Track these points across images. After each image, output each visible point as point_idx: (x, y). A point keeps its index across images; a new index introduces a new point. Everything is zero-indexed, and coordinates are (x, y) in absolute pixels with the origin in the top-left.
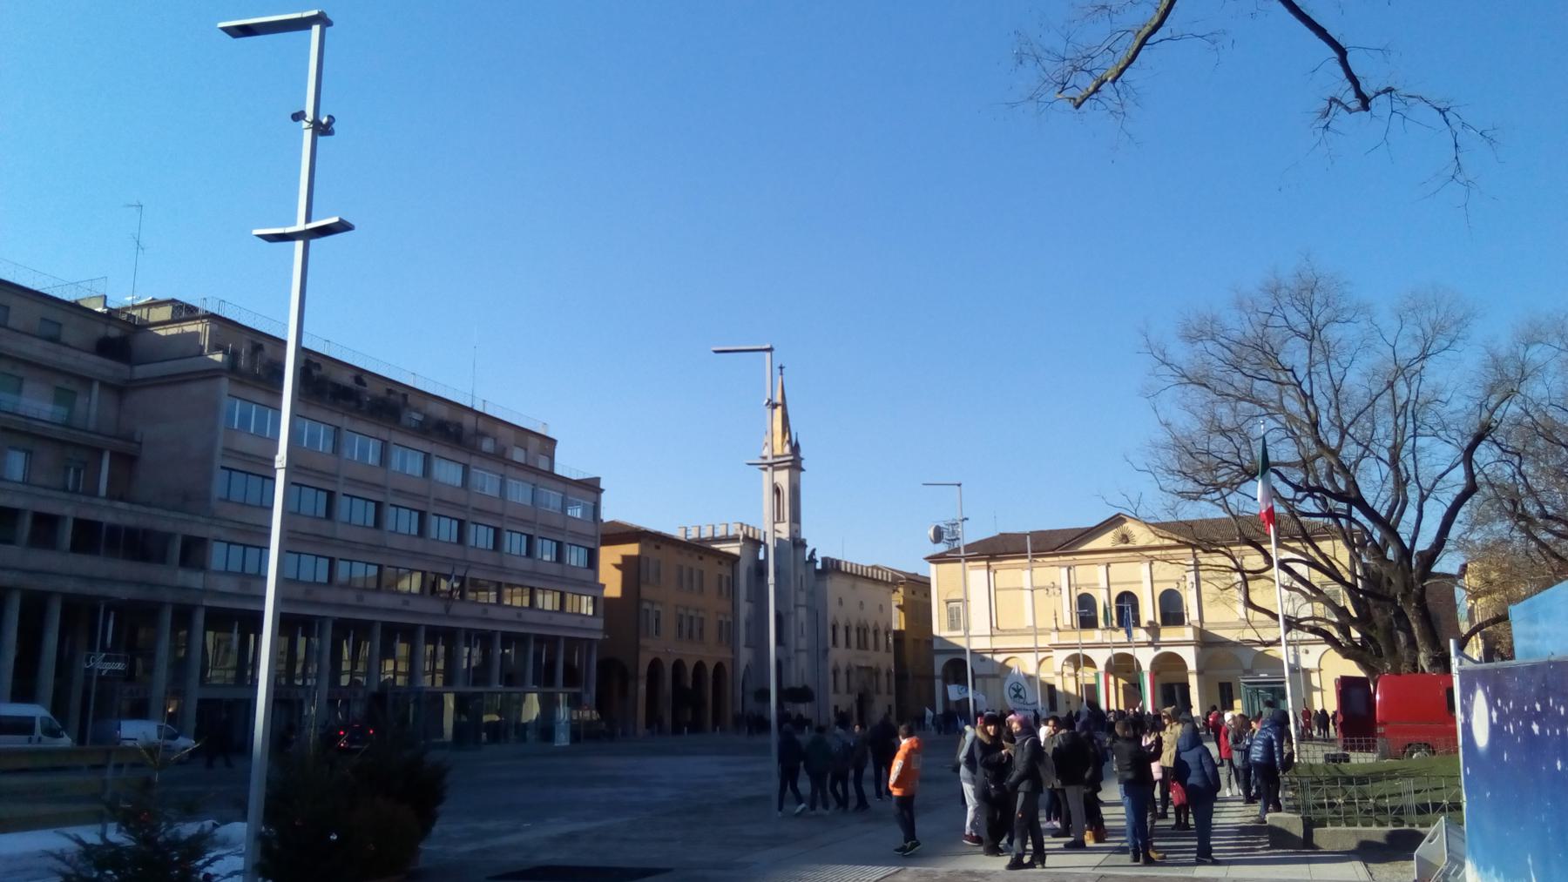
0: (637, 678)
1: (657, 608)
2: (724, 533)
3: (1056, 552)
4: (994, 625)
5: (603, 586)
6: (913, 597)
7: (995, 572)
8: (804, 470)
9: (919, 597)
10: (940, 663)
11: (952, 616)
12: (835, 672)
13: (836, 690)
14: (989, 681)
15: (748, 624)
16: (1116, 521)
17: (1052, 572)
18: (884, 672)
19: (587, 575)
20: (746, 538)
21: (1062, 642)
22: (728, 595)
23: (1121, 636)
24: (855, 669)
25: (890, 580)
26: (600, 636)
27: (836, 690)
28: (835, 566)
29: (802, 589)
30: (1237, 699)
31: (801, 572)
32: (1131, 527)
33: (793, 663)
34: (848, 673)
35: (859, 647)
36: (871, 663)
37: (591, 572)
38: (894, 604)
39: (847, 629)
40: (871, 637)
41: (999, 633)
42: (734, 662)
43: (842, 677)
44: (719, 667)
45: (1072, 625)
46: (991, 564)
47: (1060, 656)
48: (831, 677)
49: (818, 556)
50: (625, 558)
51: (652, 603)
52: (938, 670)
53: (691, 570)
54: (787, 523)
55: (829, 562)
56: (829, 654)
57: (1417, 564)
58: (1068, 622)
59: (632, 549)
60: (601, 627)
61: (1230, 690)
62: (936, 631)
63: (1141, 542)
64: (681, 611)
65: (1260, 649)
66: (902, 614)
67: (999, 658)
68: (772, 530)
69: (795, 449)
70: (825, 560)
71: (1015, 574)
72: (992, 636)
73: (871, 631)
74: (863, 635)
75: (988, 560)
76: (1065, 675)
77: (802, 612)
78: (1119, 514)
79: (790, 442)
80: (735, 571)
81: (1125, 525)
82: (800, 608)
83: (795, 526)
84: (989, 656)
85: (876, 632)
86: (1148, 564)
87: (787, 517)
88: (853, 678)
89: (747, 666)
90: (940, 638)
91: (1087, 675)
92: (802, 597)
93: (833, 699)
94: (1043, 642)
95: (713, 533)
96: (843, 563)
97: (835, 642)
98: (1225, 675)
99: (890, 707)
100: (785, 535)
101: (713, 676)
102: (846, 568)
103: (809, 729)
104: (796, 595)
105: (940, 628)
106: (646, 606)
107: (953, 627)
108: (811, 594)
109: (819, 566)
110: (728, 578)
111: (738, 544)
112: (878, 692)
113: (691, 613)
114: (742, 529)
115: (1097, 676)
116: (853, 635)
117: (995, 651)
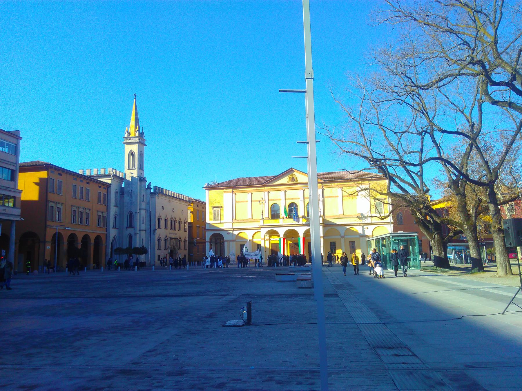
0: (45, 242)
1: (59, 206)
2: (103, 173)
3: (263, 185)
4: (234, 218)
5: (20, 192)
6: (197, 208)
7: (236, 194)
8: (146, 145)
9: (200, 208)
10: (209, 235)
11: (215, 214)
12: (159, 240)
13: (159, 248)
14: (231, 243)
15: (115, 217)
16: (290, 171)
17: (259, 194)
18: (183, 240)
19: (11, 184)
20: (115, 176)
21: (265, 225)
22: (104, 203)
23: (291, 221)
24: (169, 239)
25: (187, 200)
26: (18, 219)
27: (159, 248)
28: (160, 191)
29: (143, 202)
30: (358, 249)
31: (143, 193)
32: (296, 174)
33: (138, 236)
34: (165, 240)
35: (171, 229)
36: (177, 236)
37: (12, 183)
38: (189, 211)
39: (166, 221)
40: (177, 225)
41: (236, 221)
42: (107, 236)
43: (162, 243)
44: (98, 239)
45: (269, 218)
46: (234, 190)
47: (264, 231)
48: (157, 242)
49: (152, 186)
50: (41, 179)
51: (56, 203)
52: (208, 239)
53: (82, 188)
54: (137, 169)
55: (157, 189)
56: (156, 231)
57: (404, 193)
58: (267, 216)
59: (44, 174)
60: (19, 214)
61: (335, 245)
62: (207, 221)
63: (299, 181)
64: (74, 208)
65: (348, 227)
66: (192, 215)
67: (236, 233)
68: (131, 174)
69: (142, 135)
70: (155, 188)
71: (243, 195)
72: (233, 223)
73: (178, 221)
74: (173, 224)
75: (233, 189)
76: (265, 240)
77: (143, 212)
78: (291, 168)
79: (139, 131)
80: (108, 192)
81: (294, 173)
82: (142, 210)
83: (141, 171)
84: (231, 232)
85: (179, 223)
86: (302, 191)
87: (137, 167)
88: (168, 243)
89: (114, 237)
90: (209, 224)
91: (275, 240)
92: (143, 206)
93: (157, 252)
94: (256, 225)
95: (98, 173)
96: (164, 190)
97: (159, 226)
98: (333, 239)
99: (185, 255)
100: (136, 175)
101: (82, 242)
102: (166, 193)
103: (87, 269)
104: (140, 204)
105: (209, 220)
106: (51, 204)
107: (215, 219)
108: (148, 203)
109: (152, 191)
110: (105, 194)
111: (111, 179)
112: (180, 249)
113: (81, 210)
114: (112, 171)
115: (280, 239)
116: (169, 224)
117: (234, 230)
